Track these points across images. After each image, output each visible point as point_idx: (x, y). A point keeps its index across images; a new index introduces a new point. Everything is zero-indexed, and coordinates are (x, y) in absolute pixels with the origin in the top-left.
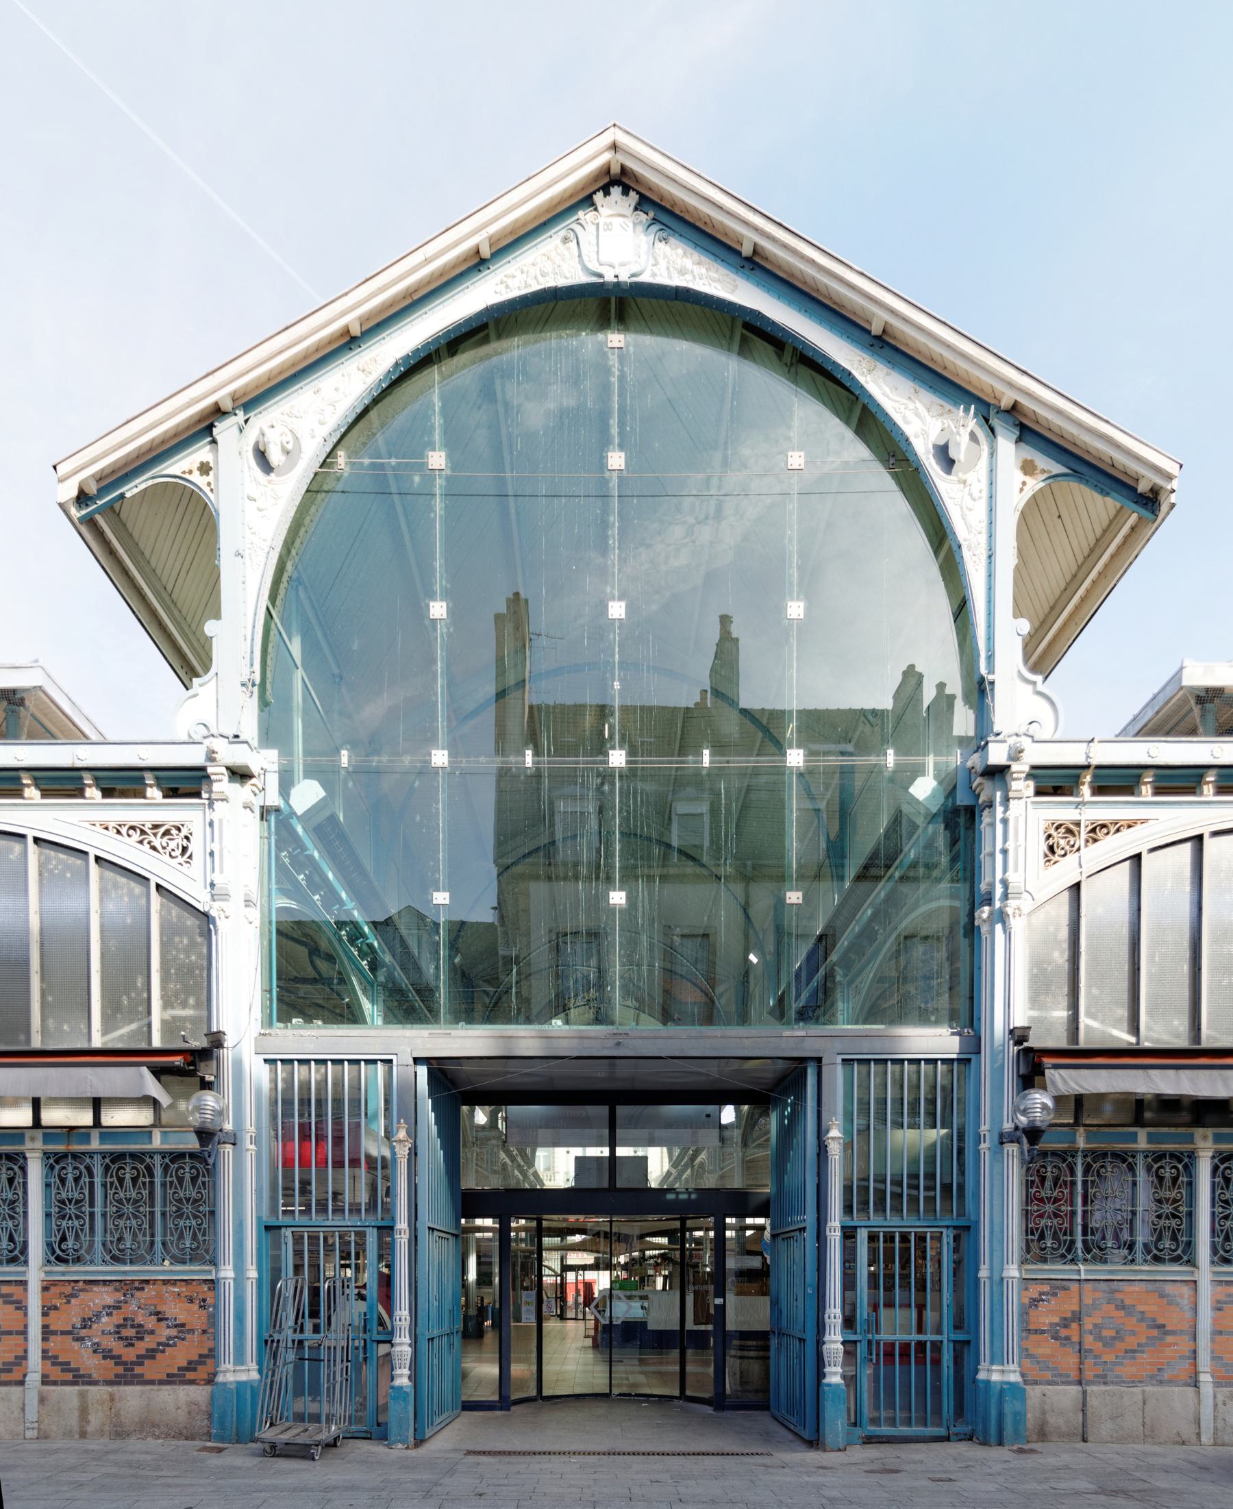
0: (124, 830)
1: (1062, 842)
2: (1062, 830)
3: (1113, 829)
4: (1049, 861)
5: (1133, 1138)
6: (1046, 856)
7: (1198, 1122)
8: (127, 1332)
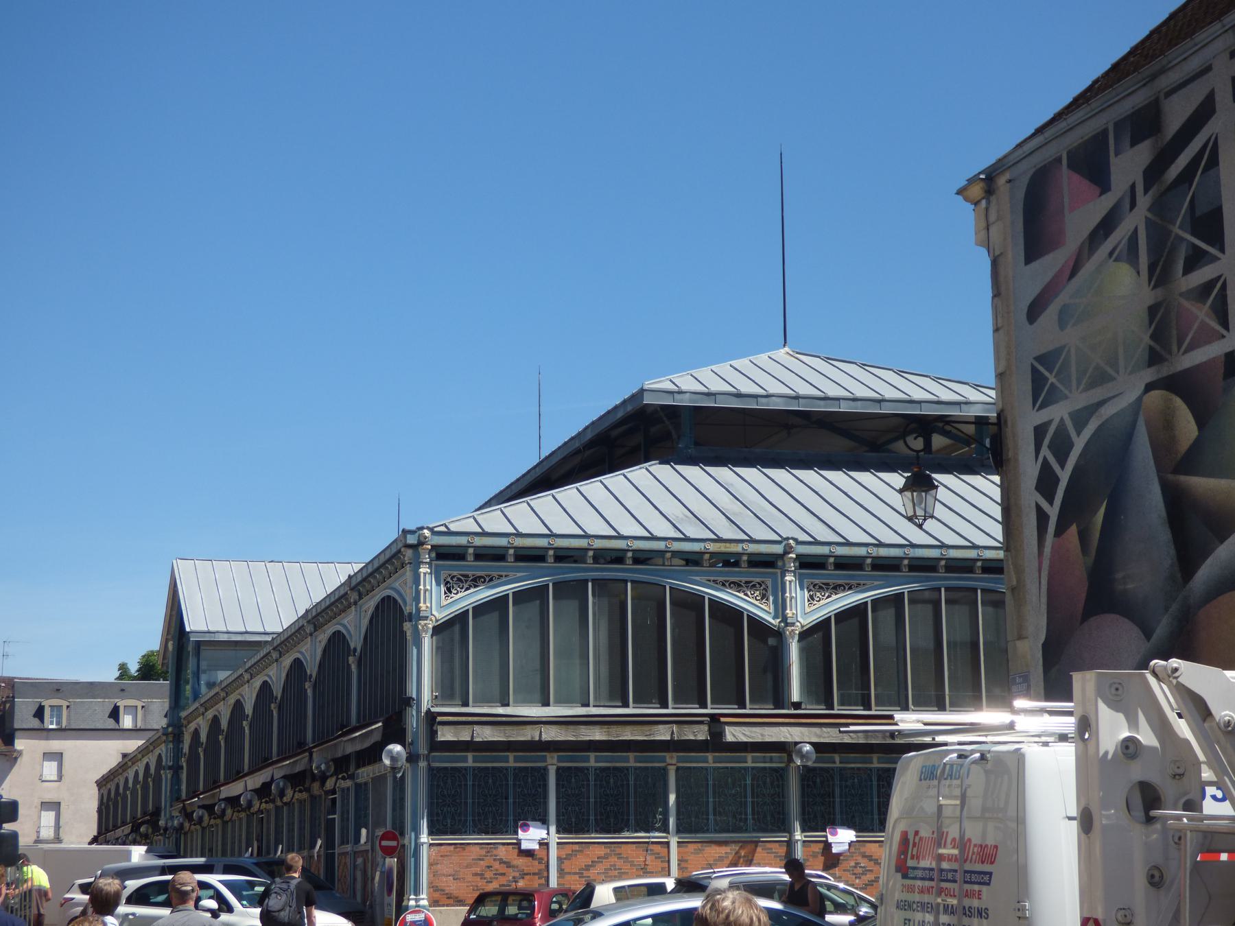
0: (727, 585)
1: (818, 594)
2: (455, 579)
3: (487, 580)
4: (448, 596)
5: (465, 760)
6: (809, 601)
7: (628, 750)
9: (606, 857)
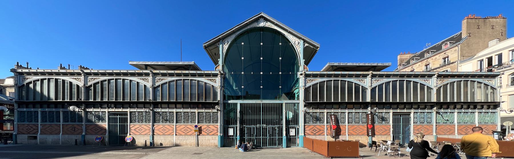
8: (164, 130)
9: (163, 127)
